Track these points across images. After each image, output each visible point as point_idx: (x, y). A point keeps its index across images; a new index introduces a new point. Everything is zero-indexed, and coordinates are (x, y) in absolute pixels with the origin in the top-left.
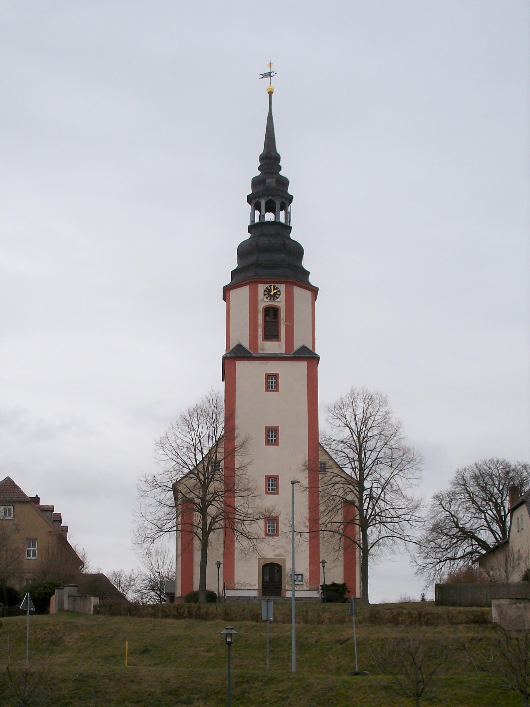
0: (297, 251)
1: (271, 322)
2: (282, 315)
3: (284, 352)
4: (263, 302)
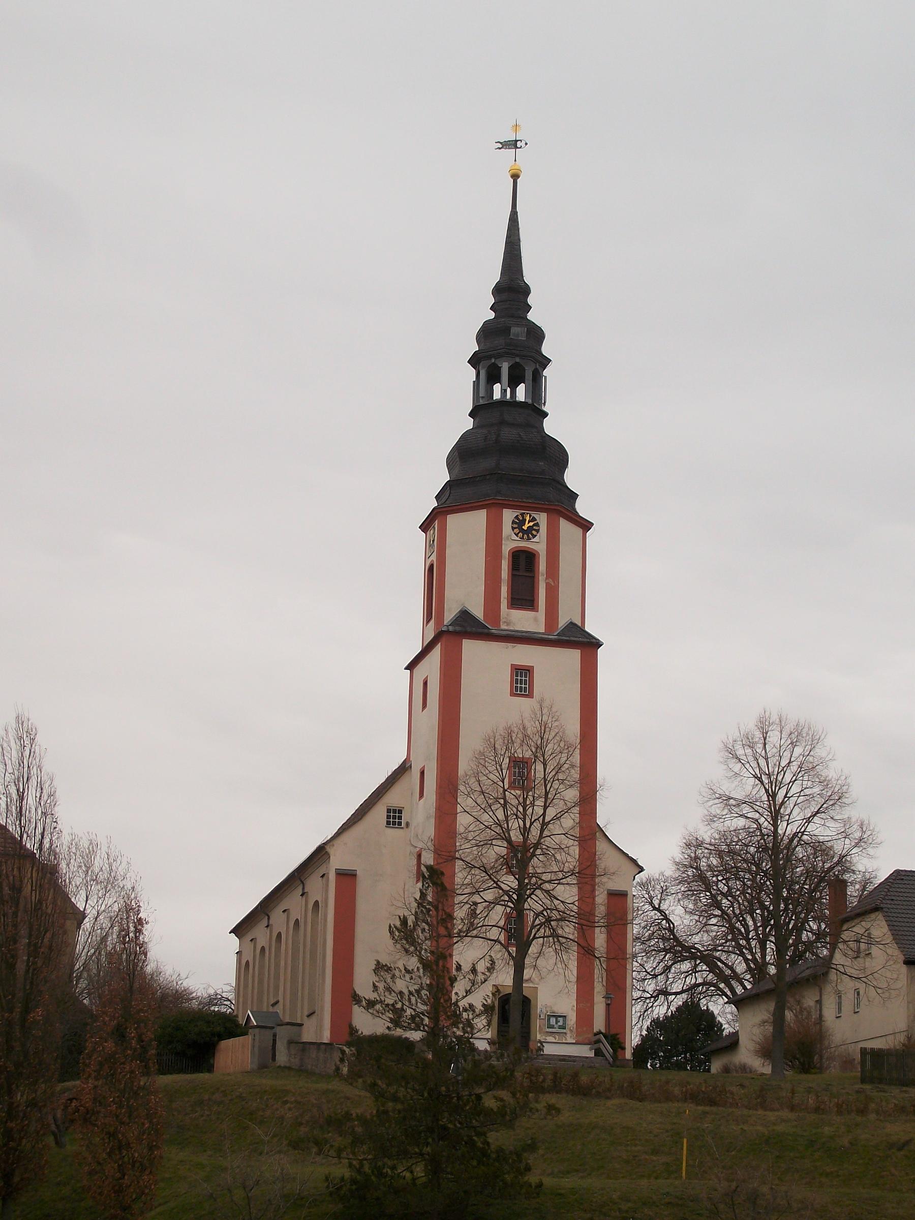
0: (557, 456)
1: (523, 577)
2: (542, 565)
3: (542, 629)
4: (511, 542)
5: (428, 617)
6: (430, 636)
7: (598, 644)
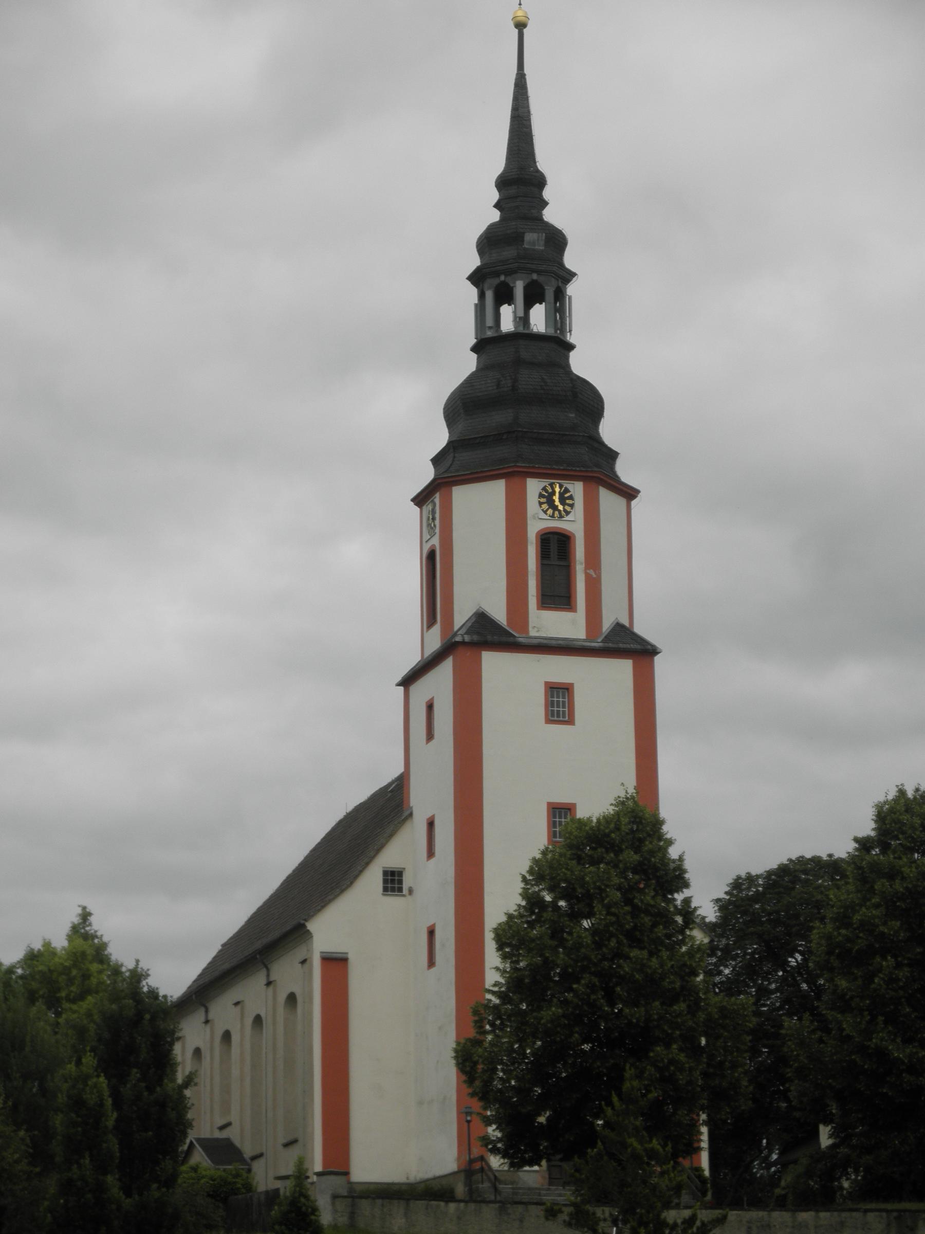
0: (587, 403)
1: (556, 565)
4: (538, 521)
5: (430, 618)
6: (435, 642)
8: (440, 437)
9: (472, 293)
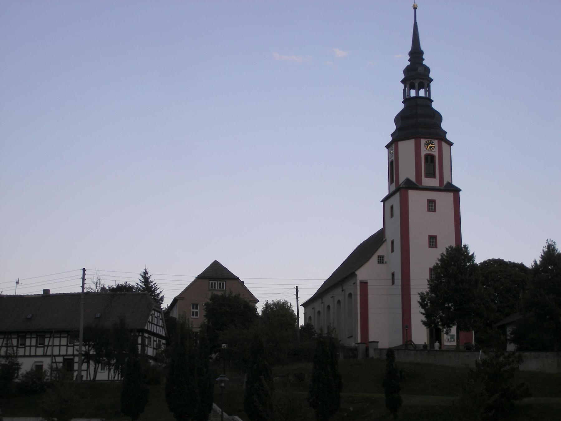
0: (437, 117)
4: (424, 151)
6: (393, 188)
7: (460, 190)
8: (393, 128)
9: (402, 86)
